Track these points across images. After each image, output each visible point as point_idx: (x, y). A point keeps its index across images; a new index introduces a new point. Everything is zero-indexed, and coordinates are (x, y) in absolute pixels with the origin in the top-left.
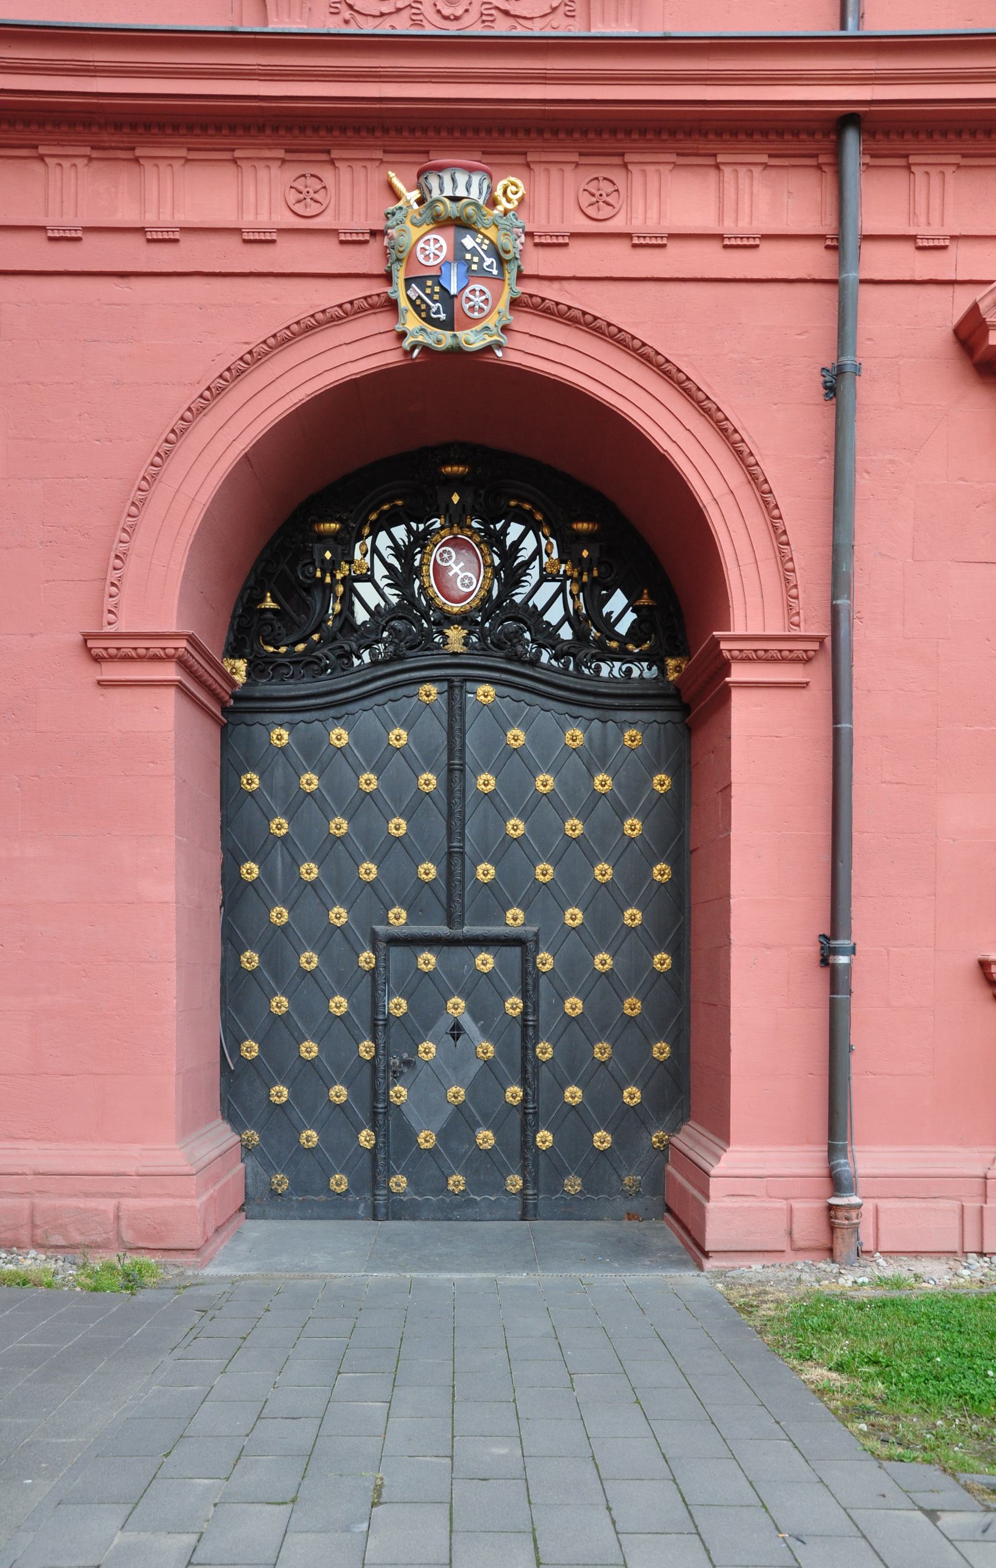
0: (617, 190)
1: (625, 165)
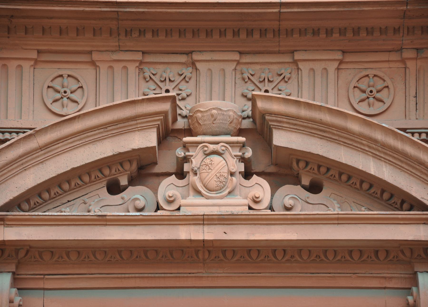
0: (82, 87)
1: (295, 62)
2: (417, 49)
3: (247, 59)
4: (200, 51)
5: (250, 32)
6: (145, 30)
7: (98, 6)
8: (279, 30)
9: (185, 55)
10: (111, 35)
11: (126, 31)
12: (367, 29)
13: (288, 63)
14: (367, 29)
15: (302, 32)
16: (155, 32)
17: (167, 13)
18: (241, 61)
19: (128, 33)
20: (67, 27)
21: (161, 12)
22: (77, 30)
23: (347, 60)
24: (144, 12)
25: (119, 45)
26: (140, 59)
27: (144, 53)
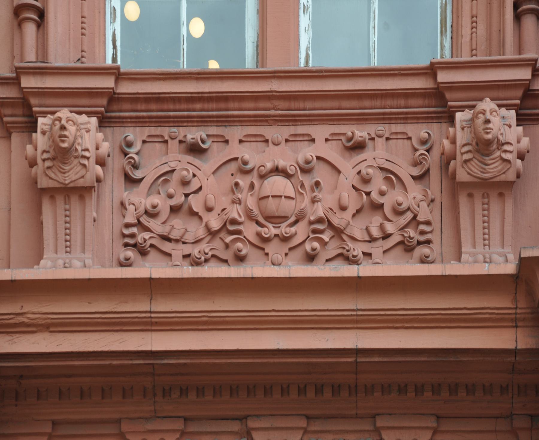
2: (531, 416)
3: (316, 426)
4: (256, 416)
5: (319, 389)
6: (187, 388)
7: (128, 358)
8: (356, 386)
9: (238, 422)
10: (145, 396)
11: (164, 390)
12: (467, 386)
13: (368, 431)
14: (467, 386)
15: (385, 389)
16: (200, 391)
17: (215, 364)
18: (309, 429)
19: (166, 392)
20: (90, 388)
21: (207, 364)
22: (103, 390)
23: (442, 428)
24: (185, 364)
25: (155, 410)
26: (181, 428)
27: (186, 419)
